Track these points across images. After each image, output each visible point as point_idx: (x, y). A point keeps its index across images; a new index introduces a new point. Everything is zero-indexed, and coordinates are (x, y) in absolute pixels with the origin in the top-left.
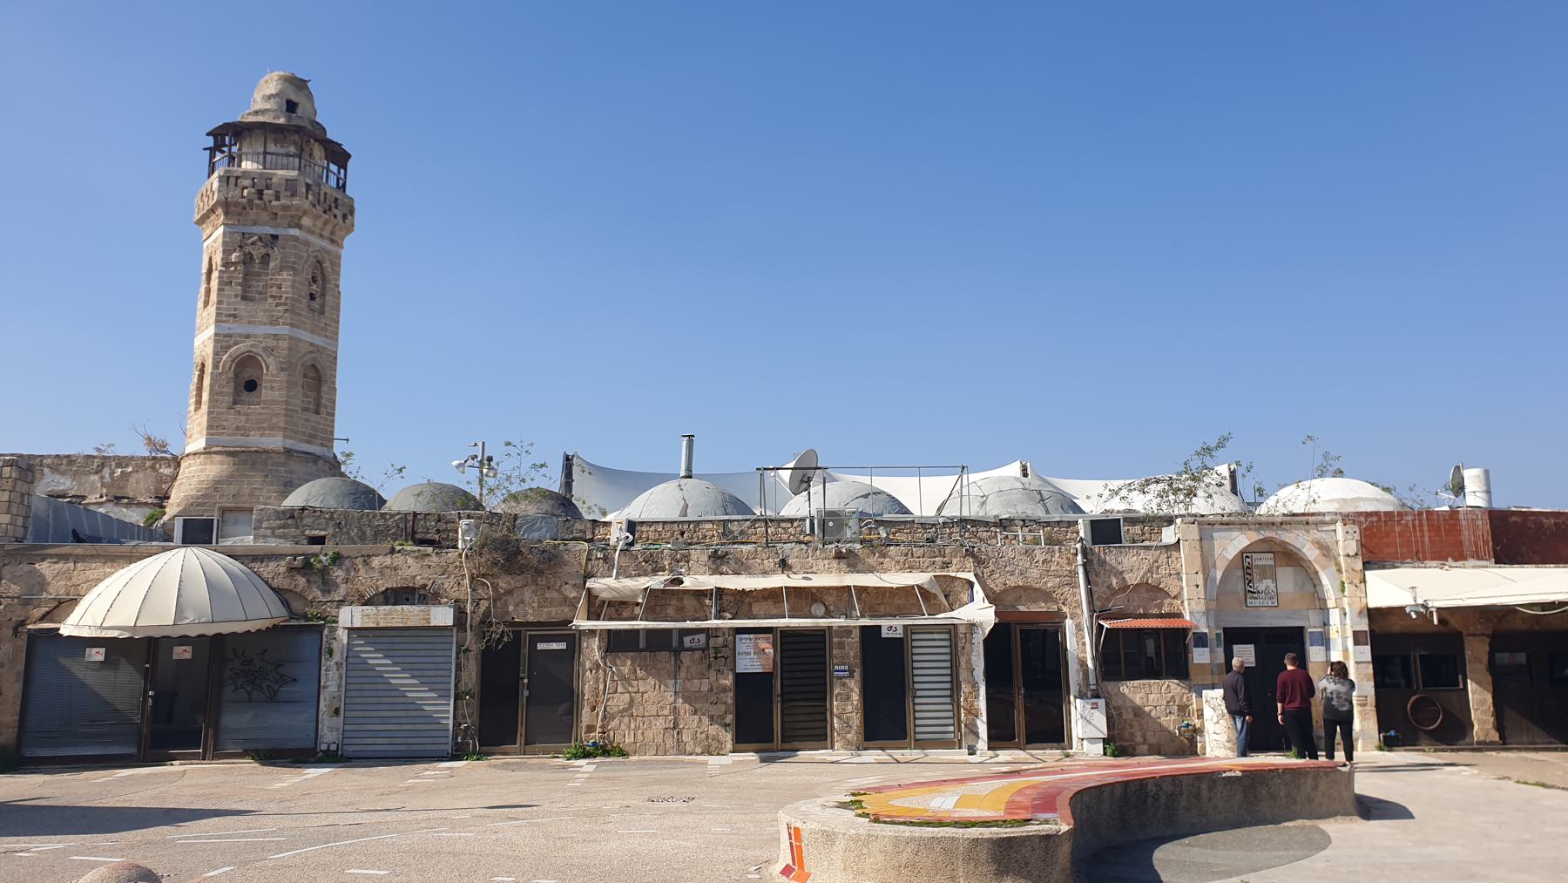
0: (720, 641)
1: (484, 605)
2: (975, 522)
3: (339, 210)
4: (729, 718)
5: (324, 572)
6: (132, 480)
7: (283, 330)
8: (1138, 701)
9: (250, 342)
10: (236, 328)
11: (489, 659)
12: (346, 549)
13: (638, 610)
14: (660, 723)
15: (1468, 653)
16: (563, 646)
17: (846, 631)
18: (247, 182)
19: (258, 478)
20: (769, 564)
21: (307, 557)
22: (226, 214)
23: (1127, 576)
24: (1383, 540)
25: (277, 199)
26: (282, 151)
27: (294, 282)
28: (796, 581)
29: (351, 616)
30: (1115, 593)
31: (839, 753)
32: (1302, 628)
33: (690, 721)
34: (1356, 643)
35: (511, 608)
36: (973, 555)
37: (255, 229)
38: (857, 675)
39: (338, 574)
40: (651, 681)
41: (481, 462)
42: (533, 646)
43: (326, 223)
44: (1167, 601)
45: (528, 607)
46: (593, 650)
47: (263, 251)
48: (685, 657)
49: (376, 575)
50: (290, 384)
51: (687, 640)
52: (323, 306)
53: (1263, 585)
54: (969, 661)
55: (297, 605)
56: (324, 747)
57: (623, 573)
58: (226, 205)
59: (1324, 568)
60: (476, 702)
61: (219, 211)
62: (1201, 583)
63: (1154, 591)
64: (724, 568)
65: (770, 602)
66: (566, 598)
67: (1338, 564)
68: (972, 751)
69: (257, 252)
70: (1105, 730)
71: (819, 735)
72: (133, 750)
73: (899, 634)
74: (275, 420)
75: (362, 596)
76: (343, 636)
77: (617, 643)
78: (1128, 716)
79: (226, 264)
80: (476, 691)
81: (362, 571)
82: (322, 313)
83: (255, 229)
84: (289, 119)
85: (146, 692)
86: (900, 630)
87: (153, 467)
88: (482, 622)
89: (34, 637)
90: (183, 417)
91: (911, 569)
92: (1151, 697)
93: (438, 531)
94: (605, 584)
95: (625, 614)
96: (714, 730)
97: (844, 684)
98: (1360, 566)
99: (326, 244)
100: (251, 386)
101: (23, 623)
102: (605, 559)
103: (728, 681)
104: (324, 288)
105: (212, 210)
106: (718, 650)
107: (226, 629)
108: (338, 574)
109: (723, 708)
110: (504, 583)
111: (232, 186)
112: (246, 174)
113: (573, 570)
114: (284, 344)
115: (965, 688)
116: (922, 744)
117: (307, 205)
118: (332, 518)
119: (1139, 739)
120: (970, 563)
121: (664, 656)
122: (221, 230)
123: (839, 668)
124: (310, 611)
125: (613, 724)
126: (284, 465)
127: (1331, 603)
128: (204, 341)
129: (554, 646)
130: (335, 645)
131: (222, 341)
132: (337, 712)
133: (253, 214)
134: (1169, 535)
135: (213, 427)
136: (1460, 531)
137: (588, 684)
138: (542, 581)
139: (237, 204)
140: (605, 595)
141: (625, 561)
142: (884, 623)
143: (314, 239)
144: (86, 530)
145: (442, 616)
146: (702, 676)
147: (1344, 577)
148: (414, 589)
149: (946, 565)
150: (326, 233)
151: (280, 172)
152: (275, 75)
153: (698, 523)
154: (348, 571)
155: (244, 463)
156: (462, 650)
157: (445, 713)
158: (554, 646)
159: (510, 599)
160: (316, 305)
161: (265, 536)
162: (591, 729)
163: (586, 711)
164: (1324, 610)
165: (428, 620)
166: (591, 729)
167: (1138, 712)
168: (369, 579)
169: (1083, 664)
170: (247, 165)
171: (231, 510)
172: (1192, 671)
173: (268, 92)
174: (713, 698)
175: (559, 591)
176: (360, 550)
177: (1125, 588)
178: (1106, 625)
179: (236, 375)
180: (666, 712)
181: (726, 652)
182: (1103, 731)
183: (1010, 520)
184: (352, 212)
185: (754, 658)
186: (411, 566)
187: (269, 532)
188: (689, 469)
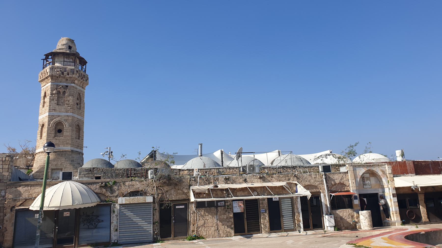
0: (229, 203)
1: (160, 195)
2: (287, 167)
3: (84, 78)
4: (233, 226)
5: (111, 187)
6: (18, 161)
8: (341, 215)
9: (59, 118)
11: (162, 212)
12: (117, 180)
13: (205, 195)
14: (213, 229)
15: (419, 198)
16: (183, 207)
17: (264, 199)
19: (63, 159)
20: (241, 180)
21: (106, 183)
22: (52, 79)
23: (336, 181)
24: (400, 169)
25: (68, 75)
26: (68, 61)
27: (73, 100)
28: (249, 185)
29: (122, 200)
30: (333, 185)
31: (264, 234)
32: (377, 194)
33: (221, 227)
34: (393, 197)
35: (168, 196)
36: (296, 177)
37: (61, 84)
38: (267, 212)
39: (115, 188)
40: (210, 216)
41: (109, 153)
42: (175, 207)
44: (346, 187)
46: (193, 208)
47: (63, 90)
48: (219, 209)
49: (127, 187)
50: (72, 130)
51: (219, 204)
52: (80, 107)
53: (367, 182)
54: (297, 206)
55: (103, 198)
56: (113, 241)
57: (200, 184)
58: (52, 76)
59: (383, 177)
60: (159, 225)
61: (50, 78)
62: (354, 182)
63: (342, 185)
64: (229, 182)
65: (242, 192)
66: (184, 192)
67: (387, 176)
69: (62, 91)
70: (334, 223)
71: (258, 230)
73: (278, 200)
74: (68, 141)
75: (123, 194)
76: (118, 206)
77: (199, 205)
78: (339, 219)
79: (52, 94)
80: (159, 222)
81: (123, 187)
82: (80, 109)
83: (61, 84)
84: (70, 51)
85: (55, 227)
86: (278, 199)
87: (25, 157)
89: (18, 211)
90: (36, 140)
91: (280, 181)
92: (344, 214)
93: (135, 174)
95: (201, 197)
96: (229, 230)
97: (264, 215)
98: (392, 176)
99: (81, 88)
100: (60, 131)
101: (14, 207)
102: (195, 180)
103: (232, 215)
104: (80, 101)
106: (228, 206)
107: (87, 206)
108: (115, 188)
110: (166, 188)
112: (58, 67)
113: (186, 184)
114: (70, 118)
115: (296, 214)
116: (286, 231)
117: (77, 77)
118: (103, 171)
119: (342, 226)
120: (295, 178)
122: (50, 84)
123: (262, 210)
124: (107, 199)
125: (200, 230)
126: (71, 155)
127: (385, 186)
128: (44, 116)
129: (181, 207)
130: (115, 210)
131: (51, 118)
132: (116, 230)
133: (60, 79)
134: (343, 169)
136: (406, 167)
137: (191, 218)
138: (177, 188)
142: (273, 197)
143: (78, 87)
144: (22, 177)
145: (149, 199)
146: (224, 214)
147: (389, 179)
148: (138, 191)
149: (289, 180)
151: (69, 67)
152: (65, 38)
153: (211, 169)
154: (118, 187)
155: (59, 155)
156: (154, 209)
157: (150, 228)
158: (181, 207)
159: (167, 193)
160: (78, 107)
161: (82, 177)
162: (193, 231)
163: (192, 226)
164: (383, 188)
166: (193, 231)
167: (341, 218)
168: (125, 189)
169: (326, 206)
170: (57, 64)
171: (54, 169)
172: (354, 206)
173: (63, 43)
174: (228, 221)
175: (182, 190)
176: (122, 180)
177: (335, 184)
178: (333, 194)
179: (55, 128)
180: (215, 225)
181: (230, 207)
182: (334, 224)
183: (296, 166)
184: (88, 79)
185: (238, 208)
186: (137, 185)
187: (83, 176)
188: (201, 154)
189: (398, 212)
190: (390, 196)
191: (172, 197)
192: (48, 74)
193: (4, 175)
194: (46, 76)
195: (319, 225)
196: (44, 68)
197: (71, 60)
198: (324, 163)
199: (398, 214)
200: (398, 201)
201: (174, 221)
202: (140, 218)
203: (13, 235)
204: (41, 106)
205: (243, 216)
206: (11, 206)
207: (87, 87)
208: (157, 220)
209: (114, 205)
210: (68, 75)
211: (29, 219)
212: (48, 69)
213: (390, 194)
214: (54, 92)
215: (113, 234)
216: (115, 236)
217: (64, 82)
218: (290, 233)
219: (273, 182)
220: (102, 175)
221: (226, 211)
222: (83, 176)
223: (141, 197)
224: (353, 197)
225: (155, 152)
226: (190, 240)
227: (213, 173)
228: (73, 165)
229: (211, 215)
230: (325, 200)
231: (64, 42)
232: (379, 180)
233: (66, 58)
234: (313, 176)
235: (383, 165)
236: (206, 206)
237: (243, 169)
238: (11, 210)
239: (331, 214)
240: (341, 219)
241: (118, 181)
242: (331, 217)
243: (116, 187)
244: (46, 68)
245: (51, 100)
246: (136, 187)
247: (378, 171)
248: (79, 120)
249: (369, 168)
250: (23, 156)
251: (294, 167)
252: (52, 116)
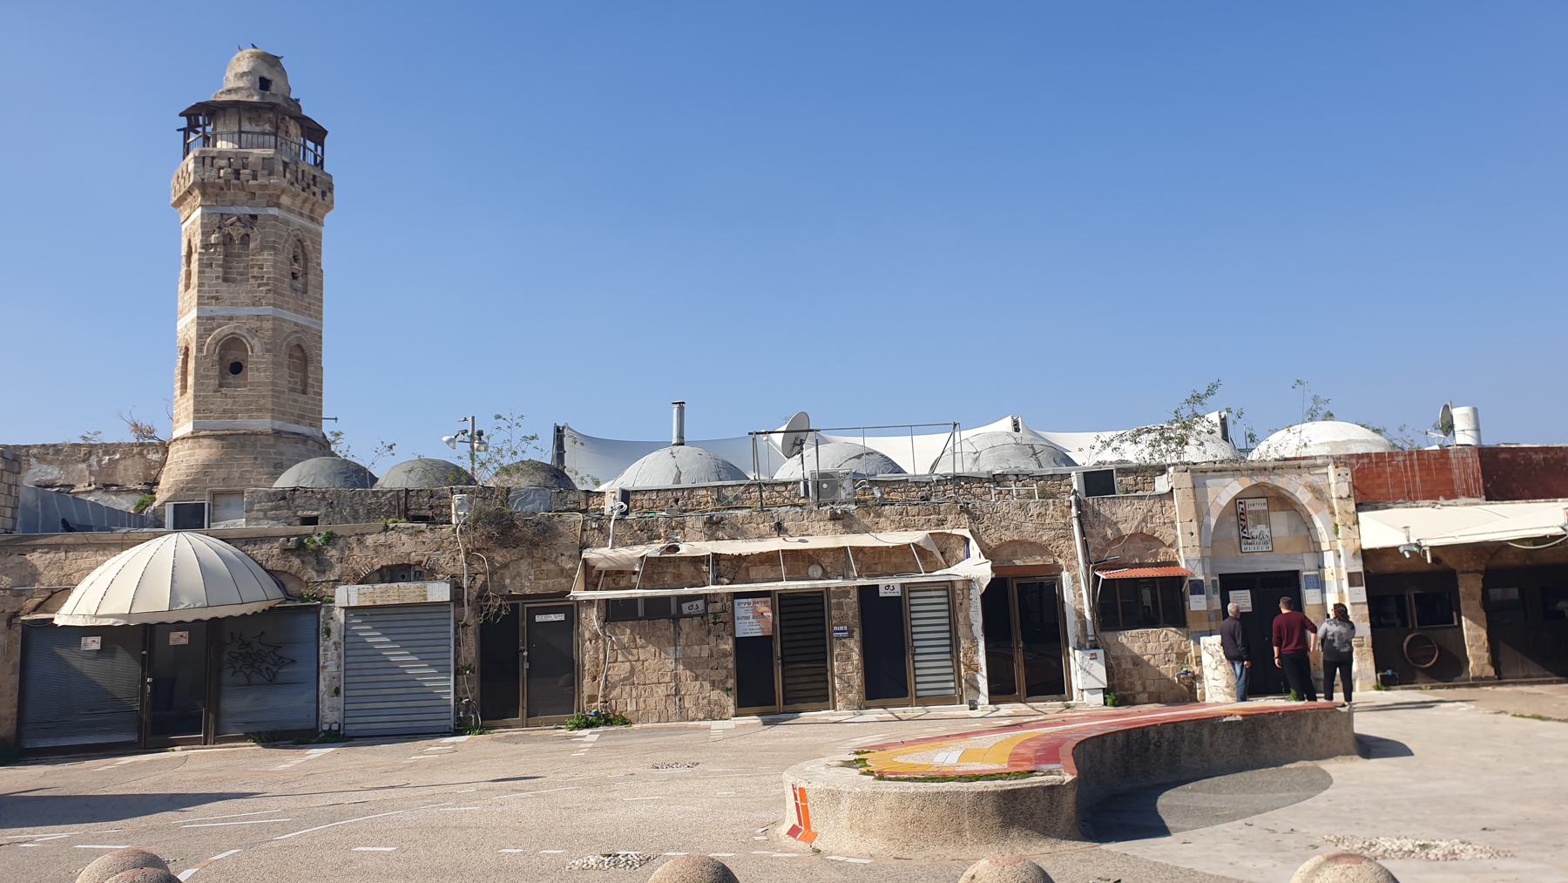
0: (718, 606)
1: (480, 579)
2: (969, 479)
3: (317, 188)
4: (731, 683)
5: (318, 552)
6: (121, 467)
7: (267, 310)
8: (1136, 650)
9: (233, 324)
10: (218, 310)
12: (339, 529)
13: (635, 579)
14: (661, 691)
15: (1462, 590)
16: (561, 617)
17: (844, 592)
18: (223, 162)
19: (247, 461)
20: (765, 528)
21: (300, 537)
22: (203, 195)
23: (1121, 527)
24: (1375, 482)
25: (255, 178)
26: (258, 129)
27: (276, 262)
28: (793, 544)
29: (347, 595)
30: (1110, 543)
31: (842, 713)
32: (1296, 573)
33: (691, 687)
34: (1352, 584)
35: (508, 581)
36: (968, 512)
37: (233, 210)
38: (857, 635)
39: (332, 553)
41: (472, 436)
42: (531, 619)
43: (305, 201)
44: (1162, 550)
45: (525, 580)
46: (591, 620)
47: (243, 231)
48: (685, 624)
49: (371, 553)
50: (276, 365)
51: (685, 606)
52: (305, 285)
53: (1256, 530)
54: (967, 617)
55: (293, 587)
56: (326, 727)
57: (619, 542)
58: (202, 186)
60: (477, 675)
61: (196, 192)
63: (1150, 540)
64: (720, 534)
65: (767, 566)
66: (562, 570)
67: (1331, 507)
68: (973, 706)
69: (237, 232)
71: (820, 696)
72: (133, 738)
73: (897, 592)
76: (340, 615)
77: (615, 612)
78: (1127, 665)
79: (206, 246)
80: (477, 665)
81: (356, 551)
82: (305, 292)
83: (233, 210)
84: (263, 96)
85: (143, 680)
86: (898, 589)
87: (141, 454)
88: (479, 597)
91: (906, 527)
92: (1149, 646)
93: (431, 507)
94: (601, 554)
95: (622, 583)
96: (715, 695)
97: (844, 645)
98: (1352, 507)
100: (237, 368)
101: (16, 615)
103: (728, 646)
104: (306, 267)
105: (189, 192)
106: (716, 615)
107: (222, 612)
108: (332, 553)
109: (724, 672)
110: (499, 556)
111: (208, 167)
112: (221, 154)
114: (268, 325)
115: (964, 644)
116: (923, 701)
117: (285, 183)
118: (323, 498)
119: (1139, 688)
120: (965, 519)
121: (663, 623)
122: (199, 211)
124: (306, 592)
125: (615, 693)
126: (273, 446)
127: (1325, 546)
128: (187, 324)
129: (553, 618)
130: (333, 625)
131: (205, 324)
132: (337, 691)
133: (230, 194)
135: (199, 410)
137: (588, 654)
138: (538, 554)
139: (213, 185)
140: (601, 565)
141: (621, 530)
142: (881, 582)
143: (293, 218)
145: (439, 592)
146: (702, 642)
147: (1337, 519)
149: (941, 523)
150: (306, 211)
151: (256, 151)
153: (692, 489)
154: (342, 550)
155: (233, 446)
156: (460, 625)
158: (553, 618)
159: (507, 573)
160: (298, 284)
161: (257, 519)
162: (592, 698)
163: (587, 681)
164: (1319, 553)
165: (425, 596)
166: (592, 698)
167: (1137, 661)
168: (364, 558)
169: (1080, 615)
171: (222, 493)
172: (1189, 619)
173: (240, 70)
174: (714, 664)
177: (1120, 538)
178: (1102, 575)
179: (221, 358)
181: (724, 617)
182: (1103, 681)
183: (1004, 475)
184: (331, 189)
185: (753, 622)
186: (405, 543)
187: (261, 515)
188: (681, 436)
191: (523, 586)
198: (1122, 461)
205: (771, 650)
207: (328, 219)
208: (470, 661)
210: (255, 178)
211: (63, 652)
214: (213, 239)
215: (327, 703)
216: (332, 709)
217: (243, 204)
220: (323, 510)
223: (412, 586)
227: (699, 504)
229: (658, 645)
231: (245, 66)
233: (250, 120)
234: (1034, 511)
235: (1316, 466)
236: (641, 613)
238: (10, 624)
240: (1135, 664)
241: (339, 533)
242: (1094, 657)
243: (334, 552)
245: (203, 266)
248: (304, 329)
249: (1261, 479)
250: (136, 450)
251: (997, 479)
252: (208, 318)
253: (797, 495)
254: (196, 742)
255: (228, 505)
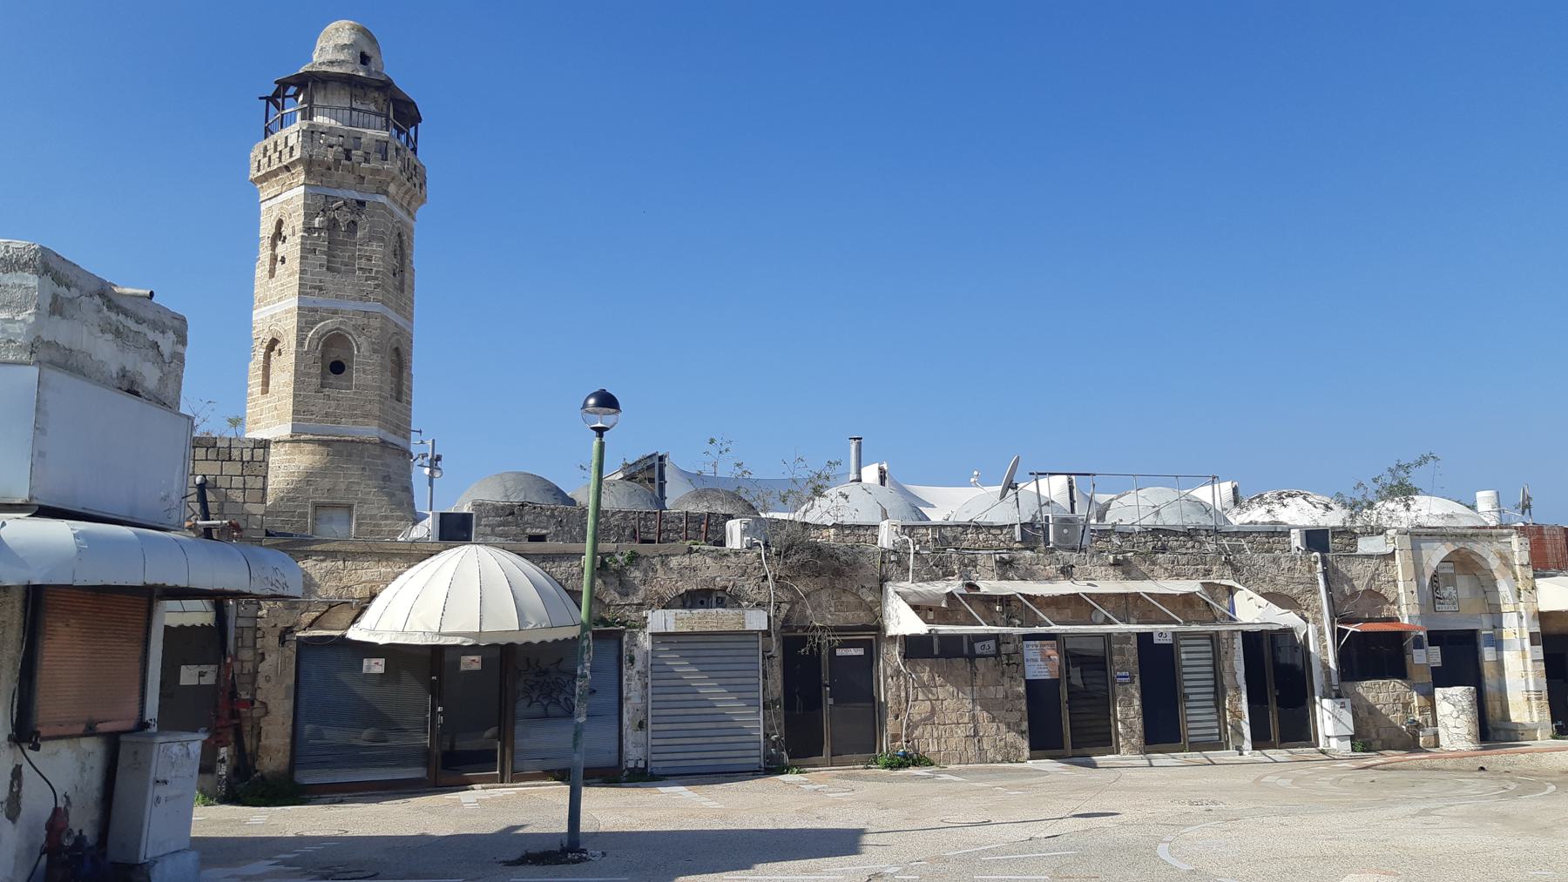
0: (1011, 647)
1: (785, 607)
2: (1168, 532)
3: (415, 175)
4: (1025, 726)
5: (620, 573)
7: (375, 307)
8: (1370, 699)
9: (337, 319)
14: (960, 732)
16: (860, 652)
17: (1125, 637)
20: (1052, 570)
22: (308, 173)
25: (367, 161)
29: (661, 620)
30: (1346, 598)
32: (1474, 632)
33: (988, 728)
35: (809, 612)
36: (1231, 564)
37: (339, 193)
39: (636, 574)
45: (825, 612)
47: (350, 217)
48: (979, 662)
54: (1232, 666)
56: (631, 765)
58: (309, 164)
59: (1504, 576)
61: (300, 168)
67: (1514, 573)
68: (1239, 749)
69: (343, 218)
72: (417, 772)
73: (1169, 640)
75: (661, 599)
76: (644, 642)
77: (914, 647)
79: (308, 229)
81: (660, 572)
83: (339, 193)
84: (369, 71)
85: (434, 709)
86: (1170, 637)
89: (306, 645)
91: (1178, 576)
96: (1011, 737)
98: (1531, 575)
100: (338, 368)
102: (898, 562)
103: (1022, 689)
106: (1004, 654)
108: (636, 574)
109: (1019, 715)
112: (330, 131)
114: (375, 323)
116: (1196, 747)
118: (552, 516)
119: (1374, 735)
120: (1228, 571)
121: (959, 662)
125: (917, 733)
129: (853, 652)
130: (636, 653)
131: (307, 316)
135: (300, 410)
137: (887, 690)
138: (839, 584)
143: (396, 209)
145: (757, 620)
146: (997, 683)
149: (1207, 573)
152: (345, 24)
154: (646, 572)
155: (339, 453)
156: (768, 657)
157: (754, 724)
158: (853, 652)
162: (896, 738)
164: (1496, 613)
166: (896, 738)
167: (1371, 710)
168: (669, 581)
169: (1325, 666)
171: (324, 506)
174: (1008, 706)
176: (656, 550)
177: (1355, 594)
178: (1351, 629)
183: (1196, 530)
185: (1041, 665)
187: (488, 530)
189: (1545, 694)
190: (1522, 639)
191: (823, 618)
192: (297, 154)
193: (249, 514)
194: (286, 160)
195: (1298, 731)
196: (268, 132)
197: (373, 107)
199: (1545, 701)
200: (1548, 659)
201: (831, 701)
202: (721, 685)
203: (289, 730)
204: (261, 271)
206: (280, 625)
207: (420, 212)
209: (633, 636)
211: (344, 677)
212: (292, 134)
213: (1521, 633)
214: (317, 222)
218: (1214, 755)
219: (1157, 578)
220: (552, 529)
221: (1003, 673)
222: (488, 530)
224: (1409, 642)
225: (661, 458)
226: (890, 766)
228: (388, 494)
230: (1324, 651)
231: (346, 38)
232: (1486, 586)
237: (1022, 531)
238: (282, 641)
239: (1338, 696)
243: (637, 574)
244: (279, 136)
245: (307, 251)
246: (706, 574)
247: (1487, 552)
253: (1012, 539)
254: (492, 780)
255: (331, 520)
